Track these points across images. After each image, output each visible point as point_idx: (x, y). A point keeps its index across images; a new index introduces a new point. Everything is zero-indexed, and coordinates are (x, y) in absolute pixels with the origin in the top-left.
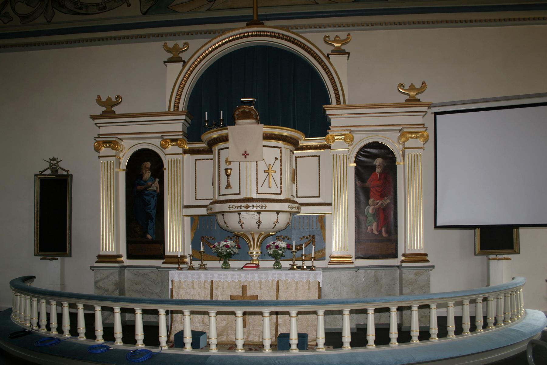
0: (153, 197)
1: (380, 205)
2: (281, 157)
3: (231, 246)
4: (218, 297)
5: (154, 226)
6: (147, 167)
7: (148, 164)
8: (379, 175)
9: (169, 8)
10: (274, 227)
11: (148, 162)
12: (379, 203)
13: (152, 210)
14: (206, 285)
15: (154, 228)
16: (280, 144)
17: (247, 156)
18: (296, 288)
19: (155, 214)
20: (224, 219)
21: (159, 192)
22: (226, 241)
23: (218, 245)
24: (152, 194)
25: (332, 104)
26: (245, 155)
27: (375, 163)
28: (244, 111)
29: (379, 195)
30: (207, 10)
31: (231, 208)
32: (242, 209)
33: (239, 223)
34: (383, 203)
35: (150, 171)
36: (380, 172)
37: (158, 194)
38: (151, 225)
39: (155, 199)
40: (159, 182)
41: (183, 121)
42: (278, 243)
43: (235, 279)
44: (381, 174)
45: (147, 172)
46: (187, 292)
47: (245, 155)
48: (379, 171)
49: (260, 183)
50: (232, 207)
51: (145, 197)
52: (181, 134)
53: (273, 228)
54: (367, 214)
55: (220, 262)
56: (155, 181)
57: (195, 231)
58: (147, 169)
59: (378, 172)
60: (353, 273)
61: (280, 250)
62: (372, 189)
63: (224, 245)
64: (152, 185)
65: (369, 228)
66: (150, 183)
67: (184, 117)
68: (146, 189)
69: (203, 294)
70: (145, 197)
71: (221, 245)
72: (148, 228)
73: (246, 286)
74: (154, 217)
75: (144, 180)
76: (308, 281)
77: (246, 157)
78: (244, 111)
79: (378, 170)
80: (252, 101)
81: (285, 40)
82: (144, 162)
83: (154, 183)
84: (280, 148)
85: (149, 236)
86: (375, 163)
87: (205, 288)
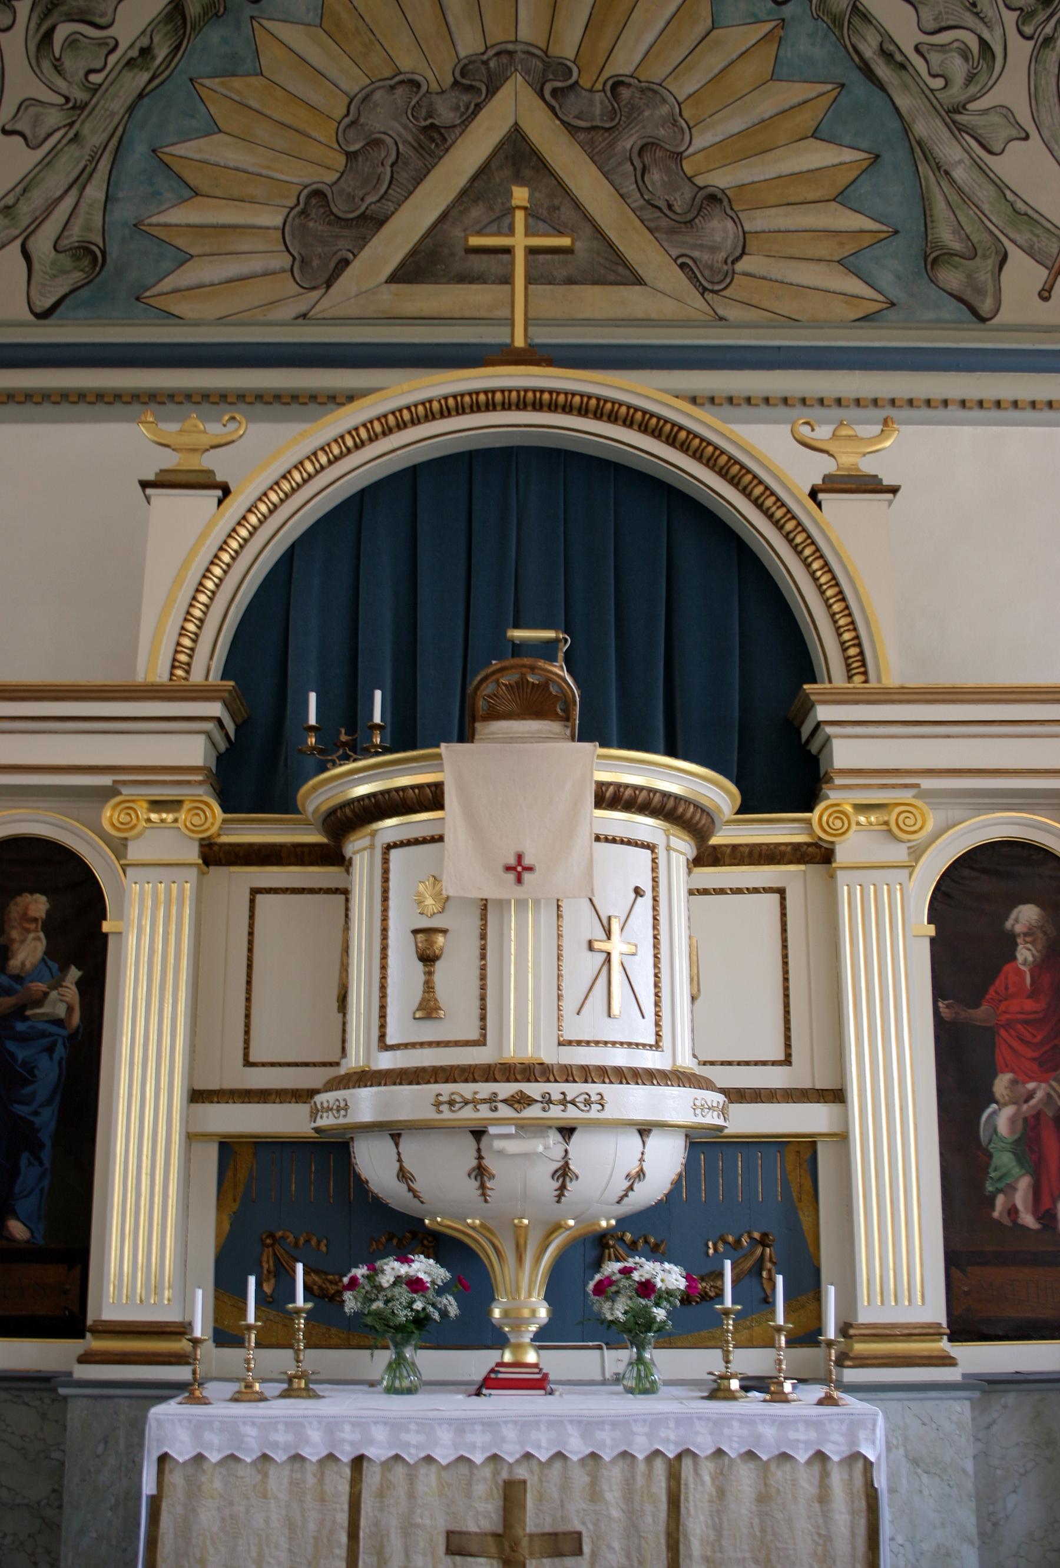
0: (50, 1050)
1: (1041, 1100)
2: (655, 887)
3: (433, 1282)
4: (385, 1540)
5: (46, 1183)
6: (32, 913)
7: (36, 901)
8: (1032, 976)
9: (144, 300)
10: (626, 1195)
11: (37, 896)
12: (1039, 1095)
13: (42, 1105)
14: (327, 1480)
15: (42, 1190)
16: (645, 826)
17: (527, 876)
18: (763, 1491)
19: (52, 1126)
20: (399, 1154)
21: (78, 1027)
22: (404, 1260)
23: (367, 1277)
24: (43, 1034)
25: (830, 681)
26: (519, 869)
27: (1013, 926)
28: (522, 683)
29: (1033, 1060)
30: (297, 318)
31: (444, 1108)
32: (496, 1109)
33: (473, 1175)
34: (1052, 1093)
35: (42, 935)
36: (1033, 962)
37: (72, 1037)
38: (29, 1174)
39: (56, 1056)
40: (79, 984)
41: (210, 726)
42: (648, 1269)
43: (473, 1447)
44: (1037, 969)
45: (32, 935)
46: (232, 1517)
47: (519, 869)
48: (1030, 959)
49: (570, 1004)
50: (451, 1103)
51: (11, 1046)
52: (200, 778)
53: (618, 1202)
54: (990, 1142)
55: (377, 1352)
56: (63, 979)
57: (235, 1206)
58: (33, 926)
59: (1025, 963)
60: (959, 1409)
61: (657, 1305)
62: (1003, 1032)
63: (398, 1280)
64: (46, 995)
65: (1000, 1200)
66: (41, 987)
67: (215, 709)
68: (19, 1012)
69: (312, 1526)
70: (11, 1046)
71: (386, 1280)
72: (17, 1190)
73: (524, 1482)
74: (46, 1137)
75: (16, 972)
76: (860, 1465)
77: (519, 880)
78: (522, 683)
79: (1025, 954)
80: (553, 643)
81: (640, 430)
82: (32, 892)
83: (57, 985)
84: (650, 847)
85: (17, 1229)
86: (1013, 926)
87: (322, 1498)
